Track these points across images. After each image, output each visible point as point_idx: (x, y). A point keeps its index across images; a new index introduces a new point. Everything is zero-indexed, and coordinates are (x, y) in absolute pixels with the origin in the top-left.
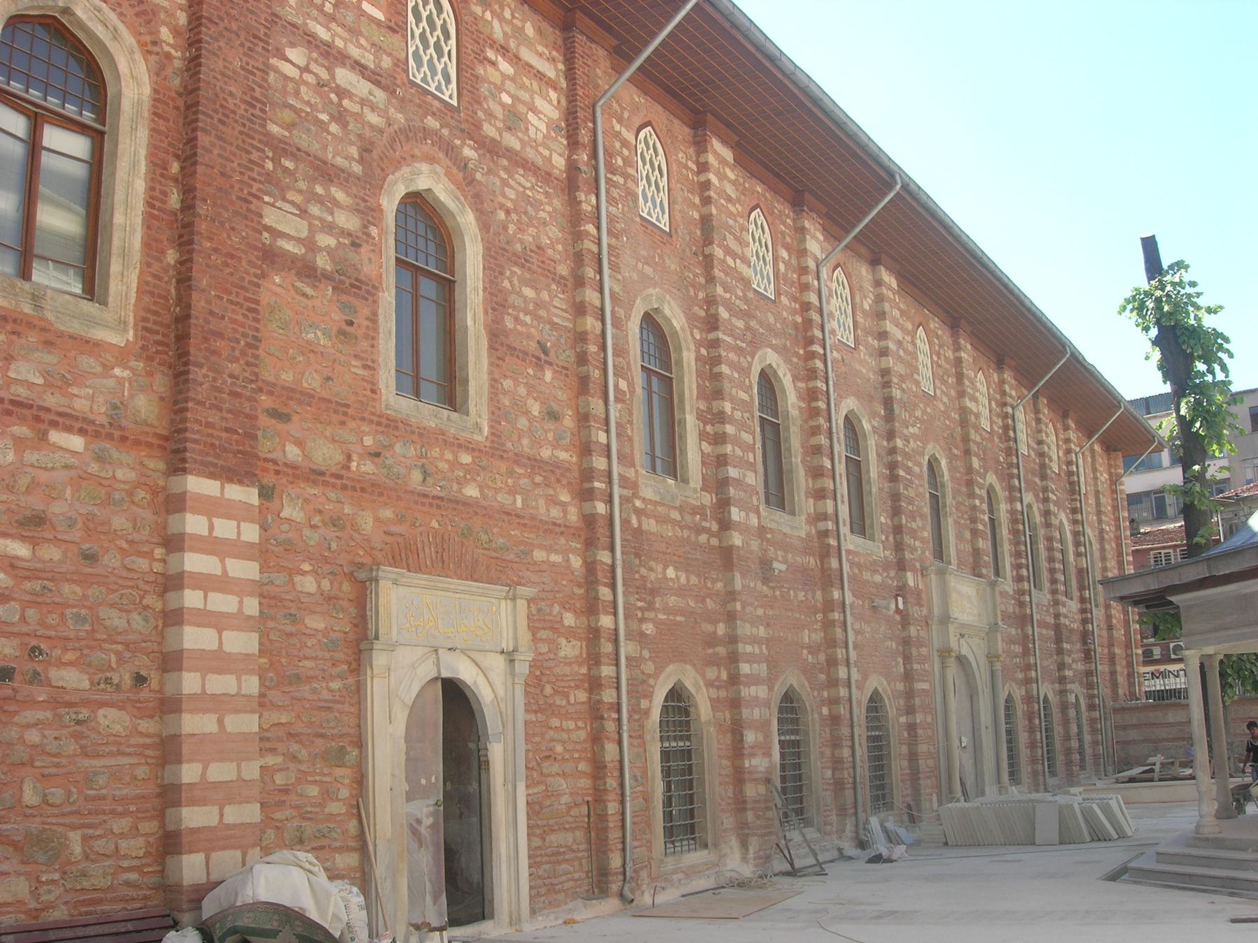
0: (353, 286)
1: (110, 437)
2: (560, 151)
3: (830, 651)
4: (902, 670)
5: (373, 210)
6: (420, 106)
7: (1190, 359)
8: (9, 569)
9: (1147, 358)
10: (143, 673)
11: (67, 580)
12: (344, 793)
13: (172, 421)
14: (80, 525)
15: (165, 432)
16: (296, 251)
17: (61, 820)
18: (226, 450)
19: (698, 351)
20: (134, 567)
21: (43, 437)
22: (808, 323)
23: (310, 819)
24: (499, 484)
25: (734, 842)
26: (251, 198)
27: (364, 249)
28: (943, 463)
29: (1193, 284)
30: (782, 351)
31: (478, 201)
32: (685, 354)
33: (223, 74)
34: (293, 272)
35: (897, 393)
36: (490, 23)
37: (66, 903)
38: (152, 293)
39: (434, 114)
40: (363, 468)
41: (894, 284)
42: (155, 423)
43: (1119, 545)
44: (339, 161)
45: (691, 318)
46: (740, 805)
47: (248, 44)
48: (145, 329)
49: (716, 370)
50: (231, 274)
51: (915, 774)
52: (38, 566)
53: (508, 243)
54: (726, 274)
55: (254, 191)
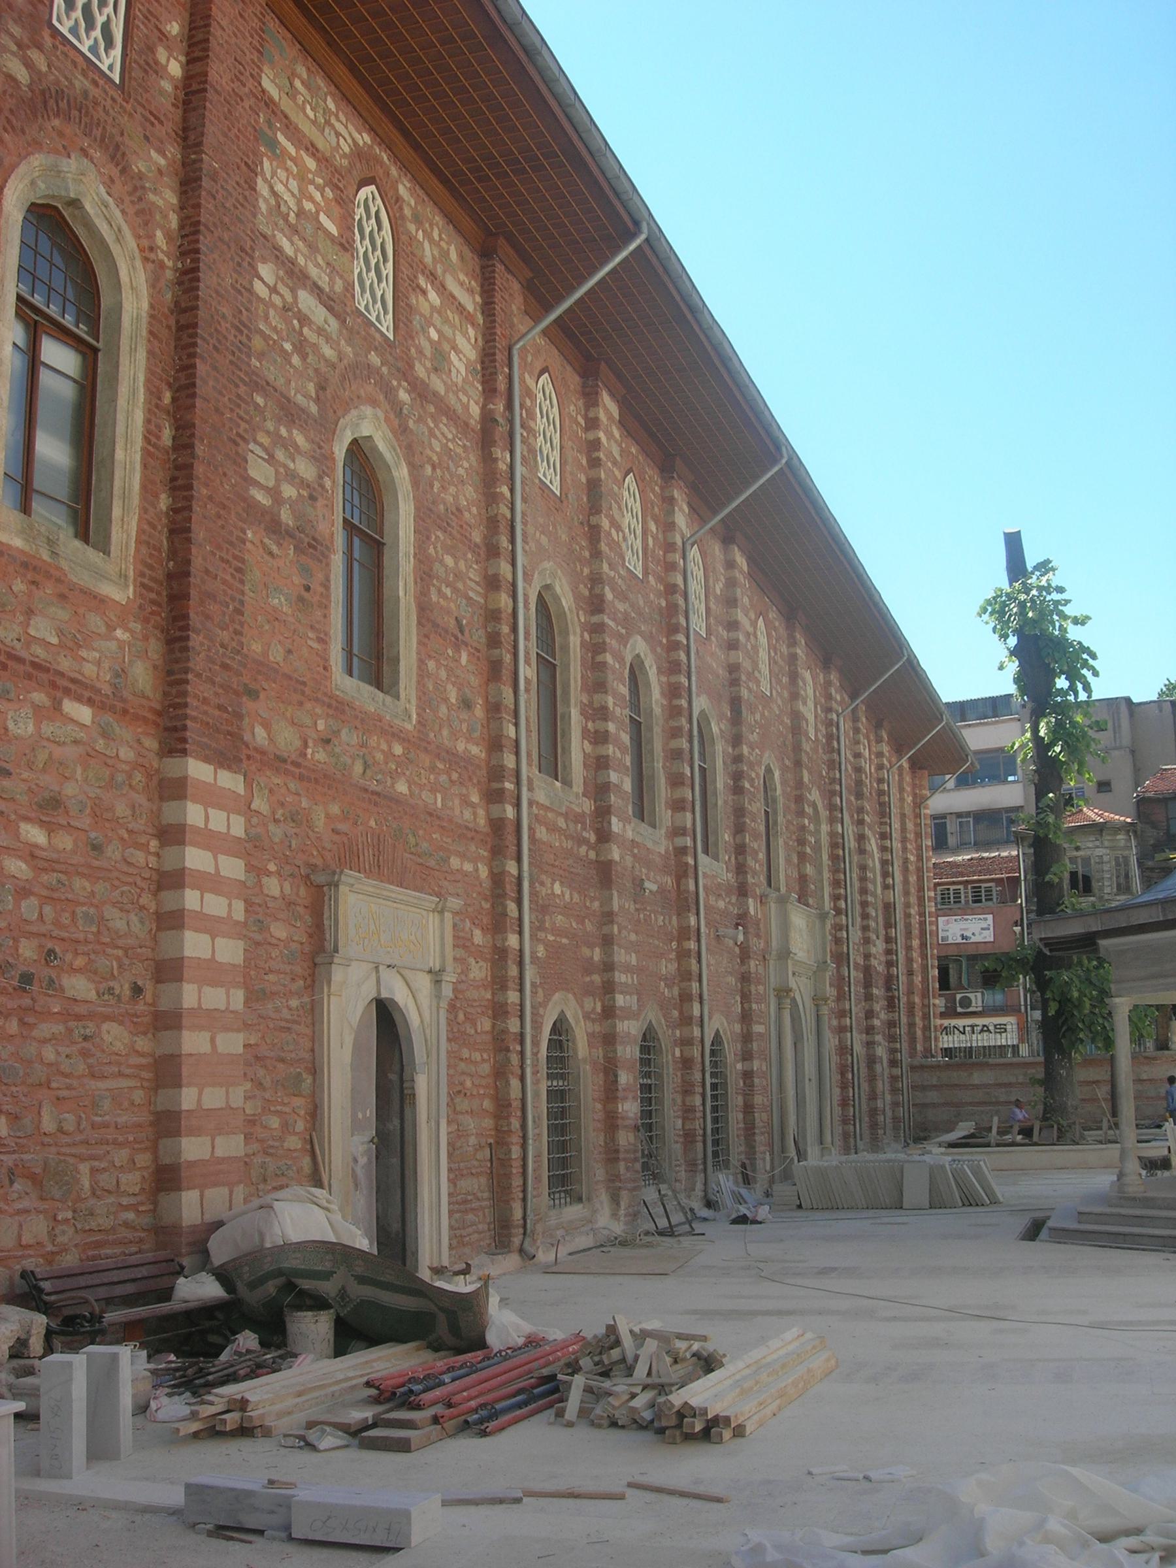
0: (313, 549)
1: (112, 709)
2: (476, 398)
3: (684, 985)
4: (740, 1010)
5: (326, 458)
6: (365, 339)
7: (1052, 675)
8: (29, 858)
9: (1001, 668)
10: (140, 983)
11: (78, 874)
12: (300, 1126)
13: (165, 694)
14: (88, 811)
15: (158, 707)
16: (264, 502)
17: (73, 1151)
18: (218, 731)
19: (582, 636)
20: (134, 861)
21: (57, 706)
22: (672, 609)
23: (271, 1155)
24: (424, 781)
25: (604, 1197)
26: (238, 440)
27: (320, 502)
28: (777, 774)
29: (1061, 590)
30: (649, 638)
31: (410, 450)
32: (572, 638)
33: (217, 292)
34: (262, 526)
35: (745, 693)
36: (422, 244)
37: (76, 1246)
38: (148, 543)
39: (376, 349)
40: (317, 756)
41: (745, 568)
42: (151, 695)
43: (920, 879)
44: (300, 399)
45: (577, 597)
46: (612, 1155)
47: (237, 259)
48: (143, 585)
49: (599, 658)
50: (223, 527)
51: (749, 1129)
52: (55, 856)
53: (433, 503)
54: (611, 549)
55: (241, 431)
